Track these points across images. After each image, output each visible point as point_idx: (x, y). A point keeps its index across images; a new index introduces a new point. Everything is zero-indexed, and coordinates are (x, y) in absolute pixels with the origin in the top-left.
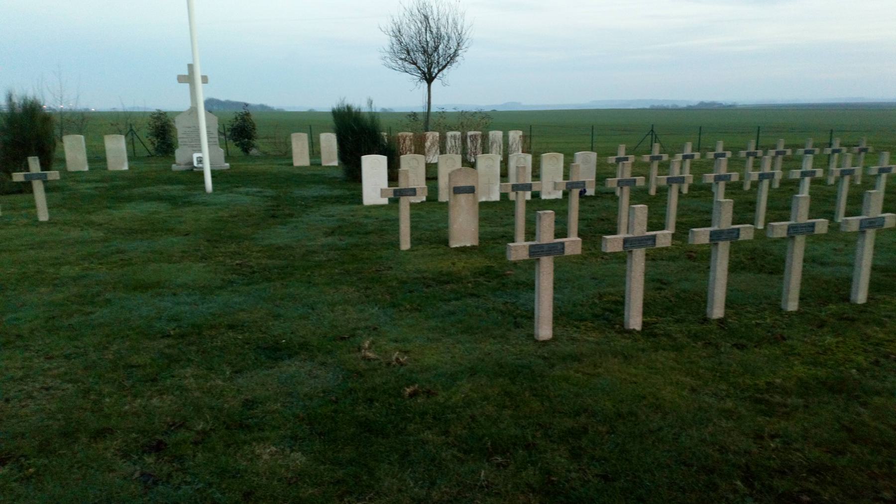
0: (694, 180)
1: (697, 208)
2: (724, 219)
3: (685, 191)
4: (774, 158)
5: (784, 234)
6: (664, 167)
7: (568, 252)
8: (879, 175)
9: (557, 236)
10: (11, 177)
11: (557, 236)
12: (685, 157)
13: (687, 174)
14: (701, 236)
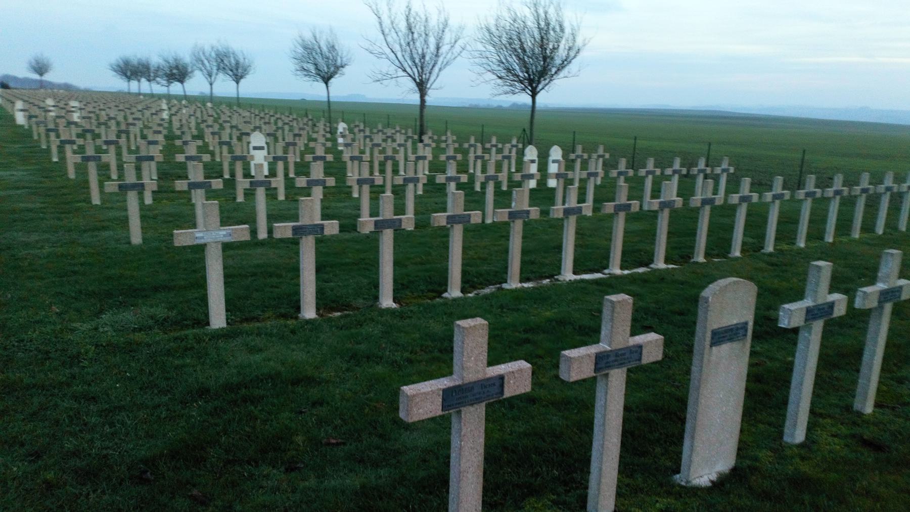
0: (336, 182)
1: (605, 193)
2: (622, 199)
3: (148, 200)
4: (597, 160)
5: (612, 211)
6: (585, 165)
7: (473, 221)
8: (647, 176)
9: (579, 202)
10: (174, 158)
11: (579, 202)
12: (599, 156)
13: (600, 170)
14: (609, 207)
